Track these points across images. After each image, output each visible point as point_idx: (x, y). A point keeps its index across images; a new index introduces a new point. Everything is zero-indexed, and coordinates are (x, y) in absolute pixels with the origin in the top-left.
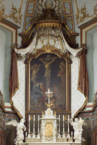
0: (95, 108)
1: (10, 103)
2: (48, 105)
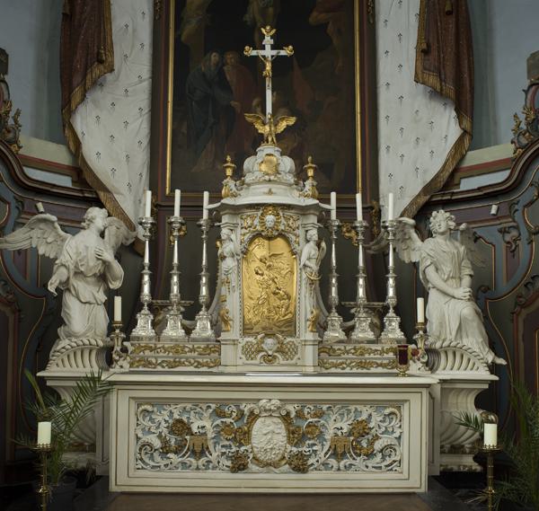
0: (525, 172)
1: (63, 148)
2: (264, 124)
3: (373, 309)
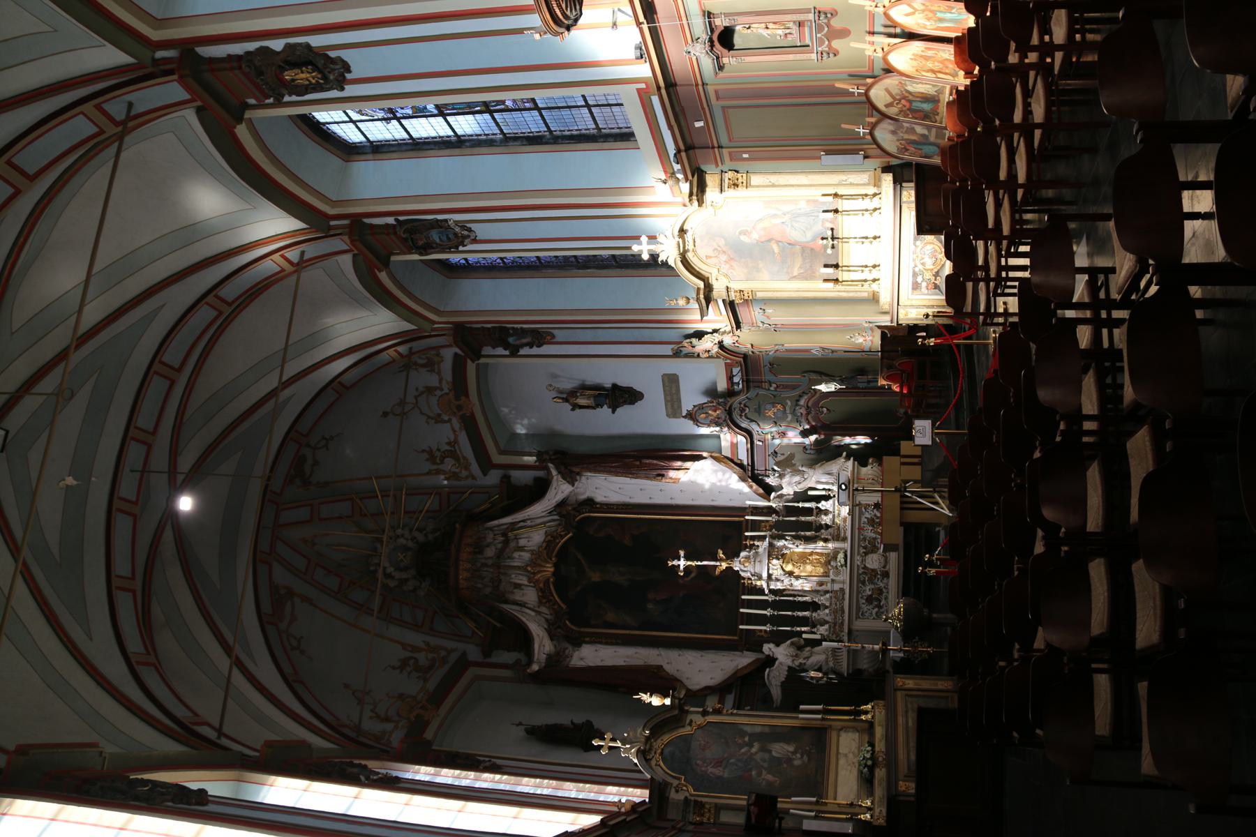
3: (817, 514)
